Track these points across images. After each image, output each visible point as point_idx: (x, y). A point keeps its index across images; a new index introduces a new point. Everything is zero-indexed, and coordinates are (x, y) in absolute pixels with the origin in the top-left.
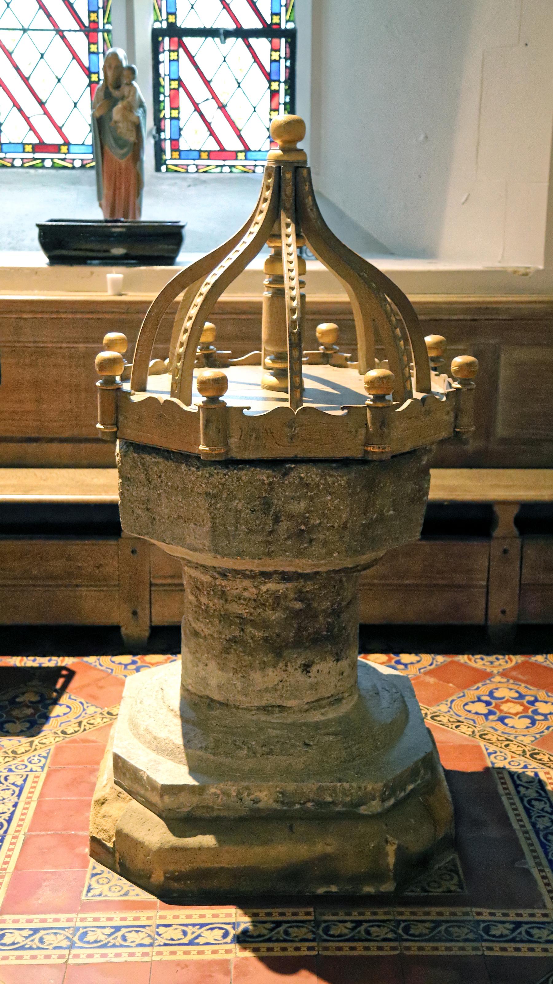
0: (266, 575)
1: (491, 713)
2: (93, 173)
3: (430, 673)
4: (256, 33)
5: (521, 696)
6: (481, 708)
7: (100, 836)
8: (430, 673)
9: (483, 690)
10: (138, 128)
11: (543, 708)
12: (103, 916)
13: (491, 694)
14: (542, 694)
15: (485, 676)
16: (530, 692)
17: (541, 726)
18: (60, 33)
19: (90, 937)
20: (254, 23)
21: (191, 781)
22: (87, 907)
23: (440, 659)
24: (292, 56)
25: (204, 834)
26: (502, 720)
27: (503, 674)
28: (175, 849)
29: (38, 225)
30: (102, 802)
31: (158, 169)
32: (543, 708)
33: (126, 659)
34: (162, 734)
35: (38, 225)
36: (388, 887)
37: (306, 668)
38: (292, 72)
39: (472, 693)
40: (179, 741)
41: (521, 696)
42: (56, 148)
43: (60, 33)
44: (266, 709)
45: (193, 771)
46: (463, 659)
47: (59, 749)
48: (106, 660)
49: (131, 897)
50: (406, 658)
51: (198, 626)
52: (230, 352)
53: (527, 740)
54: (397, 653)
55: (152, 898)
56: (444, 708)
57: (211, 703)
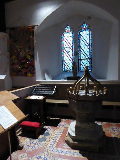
0: (84, 113)
1: (113, 130)
2: (72, 72)
3: (106, 124)
4: (88, 59)
5: (117, 128)
6: (112, 129)
7: (66, 140)
8: (106, 124)
9: (112, 127)
10: (76, 68)
11: (119, 130)
12: (65, 149)
13: (113, 128)
14: (119, 128)
15: (112, 125)
16: (118, 128)
17: (119, 132)
18: (70, 60)
19: (63, 152)
20: (88, 58)
21: (75, 136)
22: (64, 148)
23: (107, 123)
24: (92, 61)
25: (76, 142)
26: (114, 131)
27: (115, 125)
28: (73, 143)
29: (12, 101)
30: (66, 136)
31: (79, 71)
32: (119, 130)
33: (73, 120)
34: (73, 130)
35: (12, 101)
36: (98, 151)
37: (88, 124)
38: (92, 62)
39: (111, 127)
40: (74, 131)
41: (117, 128)
42: (69, 70)
43: (70, 60)
44: (84, 128)
45: (75, 135)
46: (110, 123)
47: (65, 129)
48: (71, 120)
49: (68, 148)
50: (103, 122)
51: (77, 118)
52: (28, 115)
53: (117, 134)
54: (102, 122)
55: (71, 148)
56: (107, 129)
57: (78, 127)
